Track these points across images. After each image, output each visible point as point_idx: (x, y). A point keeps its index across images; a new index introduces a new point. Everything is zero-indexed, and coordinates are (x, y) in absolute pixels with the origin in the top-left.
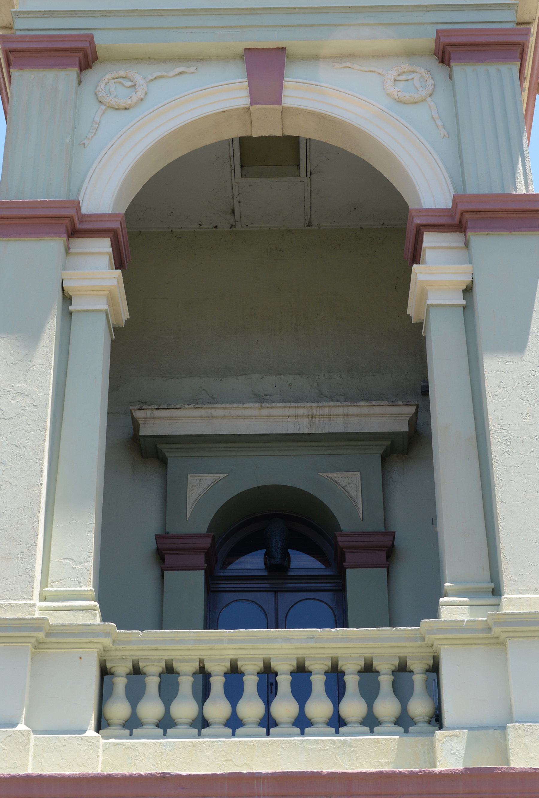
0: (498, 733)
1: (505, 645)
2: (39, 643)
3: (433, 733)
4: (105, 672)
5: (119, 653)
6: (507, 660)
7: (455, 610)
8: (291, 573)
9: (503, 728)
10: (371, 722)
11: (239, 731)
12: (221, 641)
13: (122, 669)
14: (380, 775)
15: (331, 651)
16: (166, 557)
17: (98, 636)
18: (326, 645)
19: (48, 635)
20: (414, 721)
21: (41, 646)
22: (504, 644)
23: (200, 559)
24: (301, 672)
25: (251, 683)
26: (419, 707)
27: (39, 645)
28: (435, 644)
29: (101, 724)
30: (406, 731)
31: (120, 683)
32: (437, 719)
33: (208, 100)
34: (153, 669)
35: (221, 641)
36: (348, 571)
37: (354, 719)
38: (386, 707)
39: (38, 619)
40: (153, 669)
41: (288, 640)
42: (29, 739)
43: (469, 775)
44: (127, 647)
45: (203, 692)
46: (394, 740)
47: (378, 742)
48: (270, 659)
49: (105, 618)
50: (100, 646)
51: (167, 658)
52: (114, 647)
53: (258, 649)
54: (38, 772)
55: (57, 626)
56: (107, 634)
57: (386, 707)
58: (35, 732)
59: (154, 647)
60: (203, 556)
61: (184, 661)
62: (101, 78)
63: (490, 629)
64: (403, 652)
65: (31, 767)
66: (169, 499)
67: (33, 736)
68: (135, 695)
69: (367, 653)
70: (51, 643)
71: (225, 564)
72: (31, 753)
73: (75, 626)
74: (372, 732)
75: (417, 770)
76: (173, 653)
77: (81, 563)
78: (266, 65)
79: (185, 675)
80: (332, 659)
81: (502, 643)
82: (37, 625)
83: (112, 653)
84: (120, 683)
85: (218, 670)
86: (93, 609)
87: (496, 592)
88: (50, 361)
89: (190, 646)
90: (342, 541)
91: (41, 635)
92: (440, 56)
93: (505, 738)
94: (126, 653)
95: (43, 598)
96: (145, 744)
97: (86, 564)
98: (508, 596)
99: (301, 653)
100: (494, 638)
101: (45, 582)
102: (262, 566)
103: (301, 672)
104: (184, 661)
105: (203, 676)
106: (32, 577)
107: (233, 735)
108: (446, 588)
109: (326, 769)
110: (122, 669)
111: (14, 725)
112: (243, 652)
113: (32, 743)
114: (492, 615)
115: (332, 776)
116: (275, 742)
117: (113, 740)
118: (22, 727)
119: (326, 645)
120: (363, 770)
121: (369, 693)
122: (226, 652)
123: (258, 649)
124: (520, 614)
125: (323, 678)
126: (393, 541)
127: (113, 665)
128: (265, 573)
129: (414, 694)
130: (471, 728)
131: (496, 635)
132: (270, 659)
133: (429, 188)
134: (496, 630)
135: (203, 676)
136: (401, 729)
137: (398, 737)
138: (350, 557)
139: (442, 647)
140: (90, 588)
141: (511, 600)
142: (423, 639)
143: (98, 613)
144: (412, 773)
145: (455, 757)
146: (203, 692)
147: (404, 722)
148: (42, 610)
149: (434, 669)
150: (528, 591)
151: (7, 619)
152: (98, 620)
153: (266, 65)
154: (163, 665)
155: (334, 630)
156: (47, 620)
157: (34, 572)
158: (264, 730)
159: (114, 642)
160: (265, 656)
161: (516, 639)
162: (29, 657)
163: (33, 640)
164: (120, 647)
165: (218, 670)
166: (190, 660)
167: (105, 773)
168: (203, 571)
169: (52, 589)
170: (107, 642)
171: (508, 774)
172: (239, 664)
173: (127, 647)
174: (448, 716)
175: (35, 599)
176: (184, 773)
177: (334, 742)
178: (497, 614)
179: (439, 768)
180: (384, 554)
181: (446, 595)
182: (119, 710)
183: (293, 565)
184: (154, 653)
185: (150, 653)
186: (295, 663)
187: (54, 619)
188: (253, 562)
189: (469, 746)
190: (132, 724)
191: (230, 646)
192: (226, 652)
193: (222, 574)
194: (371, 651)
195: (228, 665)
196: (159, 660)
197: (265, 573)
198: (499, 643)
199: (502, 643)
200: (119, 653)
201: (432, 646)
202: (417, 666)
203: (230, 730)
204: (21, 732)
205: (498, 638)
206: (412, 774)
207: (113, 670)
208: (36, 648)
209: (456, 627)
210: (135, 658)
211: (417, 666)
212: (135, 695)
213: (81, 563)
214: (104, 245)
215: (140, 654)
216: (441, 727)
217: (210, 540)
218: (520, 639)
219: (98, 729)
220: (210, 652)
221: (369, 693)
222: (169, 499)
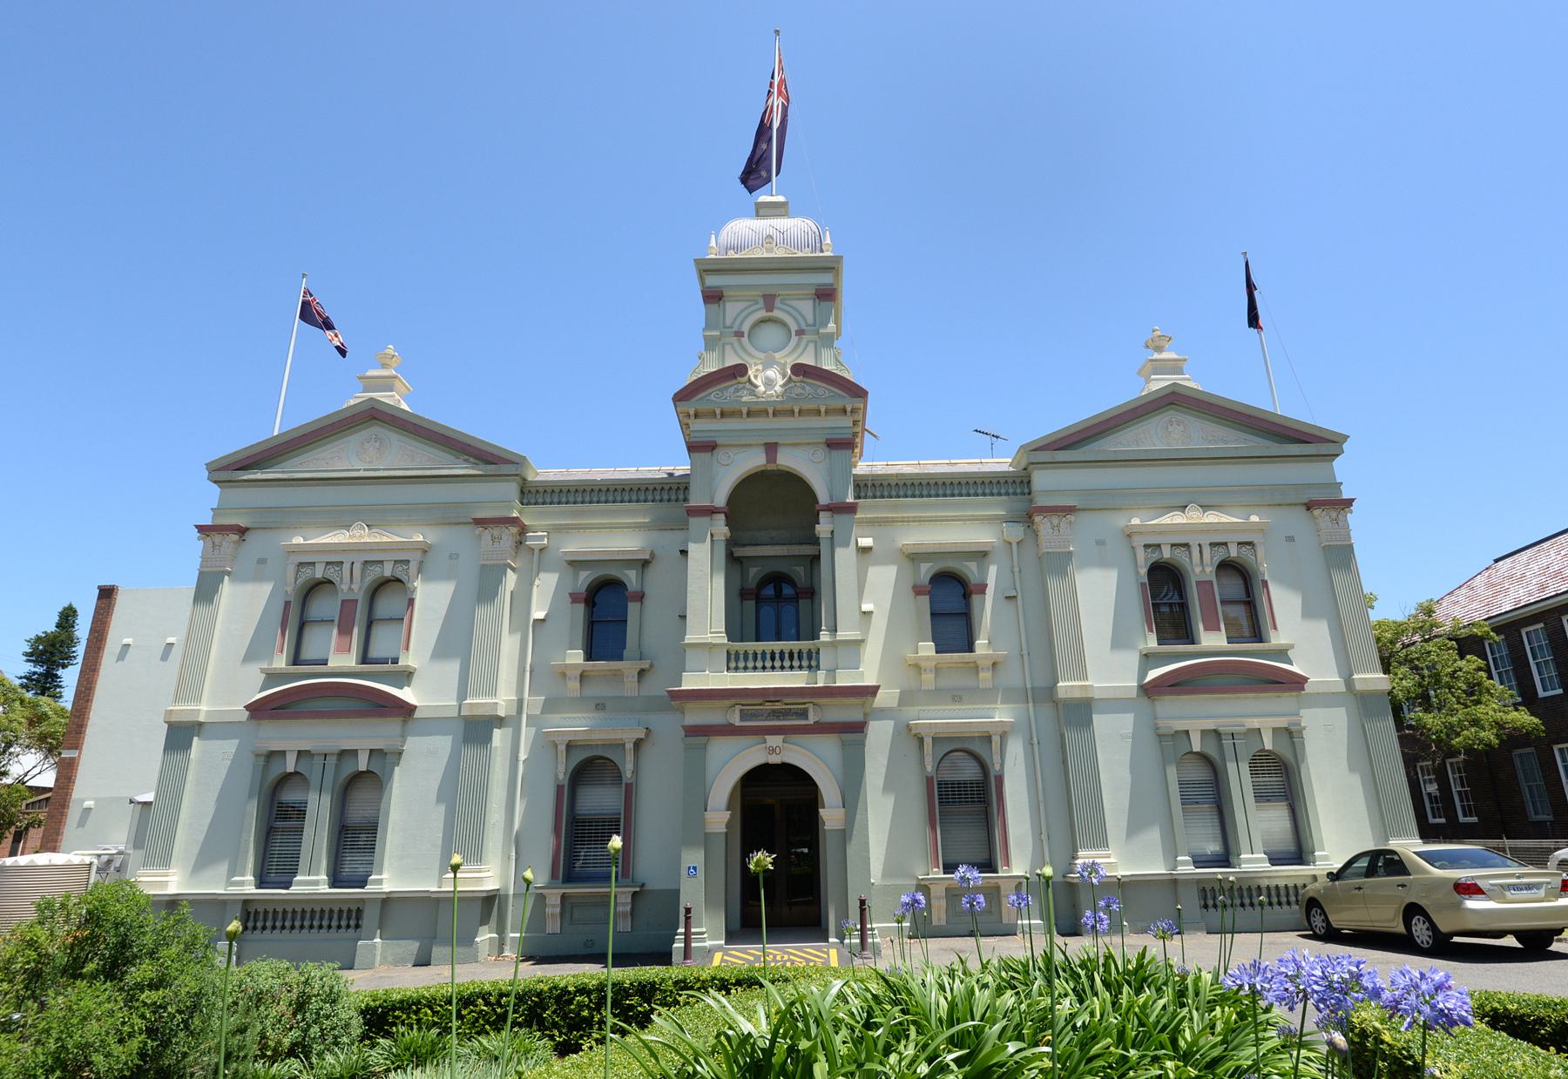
7: (825, 636)
10: (800, 667)
24: (782, 653)
32: (818, 667)
33: (755, 460)
62: (720, 454)
66: (744, 575)
68: (737, 660)
78: (771, 449)
92: (703, 739)
103: (782, 653)
105: (755, 655)
121: (782, 659)
133: (823, 498)
135: (755, 655)
146: (755, 659)
147: (810, 667)
149: (818, 653)
153: (771, 449)
182: (733, 665)
190: (736, 669)
212: (737, 660)
214: (722, 516)
221: (782, 659)
222: (744, 575)
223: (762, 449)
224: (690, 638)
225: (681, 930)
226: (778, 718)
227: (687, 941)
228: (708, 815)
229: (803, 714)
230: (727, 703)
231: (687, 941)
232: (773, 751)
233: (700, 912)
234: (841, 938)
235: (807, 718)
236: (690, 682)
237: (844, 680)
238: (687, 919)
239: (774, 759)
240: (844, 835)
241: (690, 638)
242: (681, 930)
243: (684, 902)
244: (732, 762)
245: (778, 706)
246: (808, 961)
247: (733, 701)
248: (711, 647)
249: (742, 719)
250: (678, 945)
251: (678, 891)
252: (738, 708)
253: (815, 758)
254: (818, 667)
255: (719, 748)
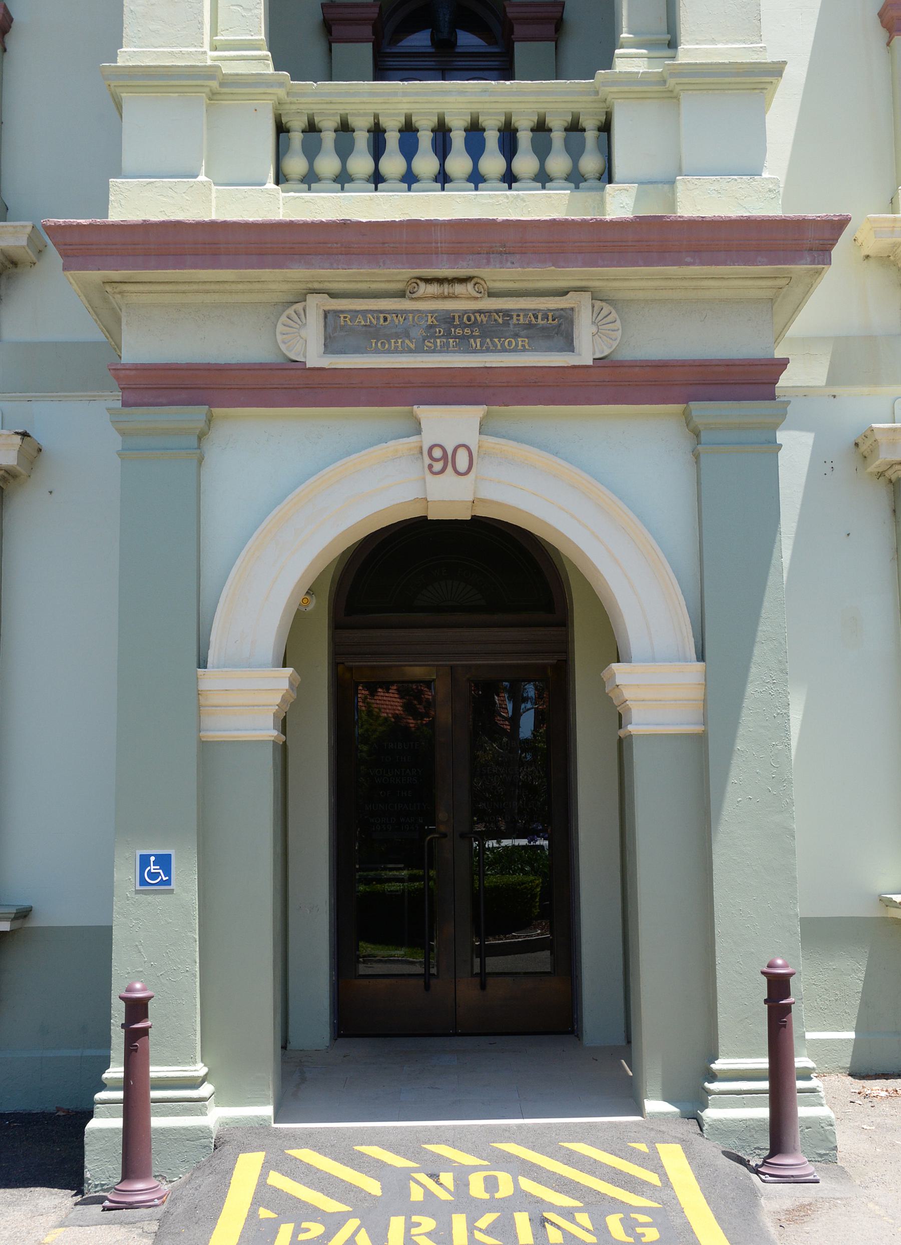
0: (666, 187)
1: (679, 100)
2: (214, 94)
3: (603, 189)
4: (281, 129)
5: (294, 107)
6: (679, 114)
7: (630, 61)
8: (458, 50)
9: (672, 183)
11: (414, 186)
12: (395, 94)
13: (297, 124)
14: (553, 223)
15: (504, 106)
16: (333, 28)
17: (272, 86)
18: (501, 99)
19: (222, 85)
20: (284, 731)
21: (215, 97)
22: (677, 98)
23: (368, 31)
25: (425, 138)
26: (590, 163)
27: (213, 95)
28: (609, 99)
29: (280, 178)
30: (577, 187)
31: (297, 137)
32: (607, 175)
34: (328, 124)
35: (395, 94)
36: (517, 45)
37: (527, 176)
38: (558, 163)
39: (210, 66)
40: (328, 124)
41: (461, 93)
42: (210, 190)
43: (640, 223)
44: (303, 100)
45: (378, 149)
46: (565, 194)
47: (550, 197)
48: (444, 114)
49: (277, 68)
50: (275, 98)
51: (342, 112)
52: (288, 100)
53: (433, 102)
54: (221, 218)
55: (230, 75)
56: (281, 85)
57: (558, 163)
58: (215, 184)
59: (328, 99)
60: (371, 27)
61: (359, 115)
63: (665, 82)
64: (576, 107)
65: (214, 214)
67: (214, 188)
69: (541, 108)
70: (225, 93)
71: (395, 41)
72: (214, 203)
73: (249, 75)
74: (544, 188)
75: (589, 218)
76: (348, 107)
77: (251, 10)
79: (361, 130)
80: (506, 114)
81: (675, 97)
82: (210, 73)
83: (287, 107)
84: (297, 137)
85: (392, 125)
86: (264, 58)
87: (672, 44)
88: (195, 976)
89: (365, 99)
90: (511, 12)
91: (214, 84)
92: (192, 416)
93: (674, 193)
94: (301, 107)
95: (215, 48)
96: (324, 198)
97: (256, 11)
98: (685, 47)
99: (476, 108)
100: (666, 92)
101: (214, 31)
102: (429, 43)
104: (359, 115)
106: (201, 23)
107: (409, 190)
108: (621, 40)
109: (501, 218)
110: (297, 124)
111: (196, 176)
112: (418, 106)
113: (214, 195)
114: (668, 65)
115: (507, 224)
116: (450, 196)
117: (292, 194)
118: (202, 178)
119: (501, 99)
120: (538, 218)
122: (400, 106)
123: (433, 102)
124: (696, 64)
125: (496, 134)
126: (562, 13)
127: (288, 119)
128: (433, 50)
129: (590, 144)
130: (641, 183)
131: (670, 89)
132: (444, 114)
134: (671, 82)
136: (572, 185)
137: (569, 192)
138: (518, 30)
139: (616, 101)
140: (261, 36)
141: (688, 50)
142: (597, 93)
143: (270, 62)
144: (584, 221)
145: (624, 210)
146: (378, 149)
147: (575, 178)
148: (215, 59)
149: (606, 128)
150: (705, 42)
151: (179, 66)
152: (271, 70)
154: (338, 119)
155: (508, 83)
156: (219, 67)
157: (203, 17)
158: (439, 185)
159: (288, 94)
160: (439, 111)
161: (690, 92)
162: (204, 106)
163: (207, 90)
164: (294, 100)
165: (392, 125)
166: (365, 115)
167: (288, 219)
168: (371, 44)
169: (222, 38)
170: (281, 93)
171: (677, 222)
172: (414, 119)
173: (303, 100)
174: (619, 169)
175: (206, 48)
176: (364, 220)
177: (507, 197)
178: (673, 64)
179: (608, 218)
180: (553, 27)
181: (622, 47)
182: (296, 165)
183: (459, 43)
184: (328, 106)
185: (325, 106)
186: (468, 119)
187: (227, 69)
188: (420, 40)
189: (637, 200)
190: (310, 179)
191: (405, 99)
192: (400, 106)
193: (388, 50)
194: (545, 105)
195: (403, 119)
196: (334, 115)
197: (433, 50)
198: (672, 97)
199: (675, 97)
200: (294, 107)
201: (605, 101)
202: (590, 123)
203: (406, 185)
204: (202, 182)
205: (671, 91)
206: (584, 222)
207: (289, 125)
208: (210, 99)
209: (631, 79)
210: (310, 112)
211: (590, 123)
213: (251, 10)
215: (315, 108)
216: (610, 181)
217: (377, 10)
218: (695, 92)
219: (277, 182)
220: (386, 106)
223: (699, 729)
224: (130, 55)
225: (115, 1072)
226: (464, 345)
227: (134, 1109)
228: (211, 680)
229: (558, 330)
230: (278, 280)
231: (134, 1109)
232: (442, 460)
233: (178, 1017)
234: (692, 1103)
235: (569, 346)
236: (132, 202)
237: (702, 200)
238: (135, 1038)
239: (450, 497)
240: (701, 757)
241: (130, 55)
242: (115, 1072)
243: (128, 976)
244: (299, 501)
245: (464, 301)
246: (598, 1206)
247: (298, 275)
248: (208, 88)
249: (330, 345)
250: (105, 1124)
251: (110, 928)
252: (315, 305)
253: (591, 494)
254: (607, 175)
255: (252, 451)
